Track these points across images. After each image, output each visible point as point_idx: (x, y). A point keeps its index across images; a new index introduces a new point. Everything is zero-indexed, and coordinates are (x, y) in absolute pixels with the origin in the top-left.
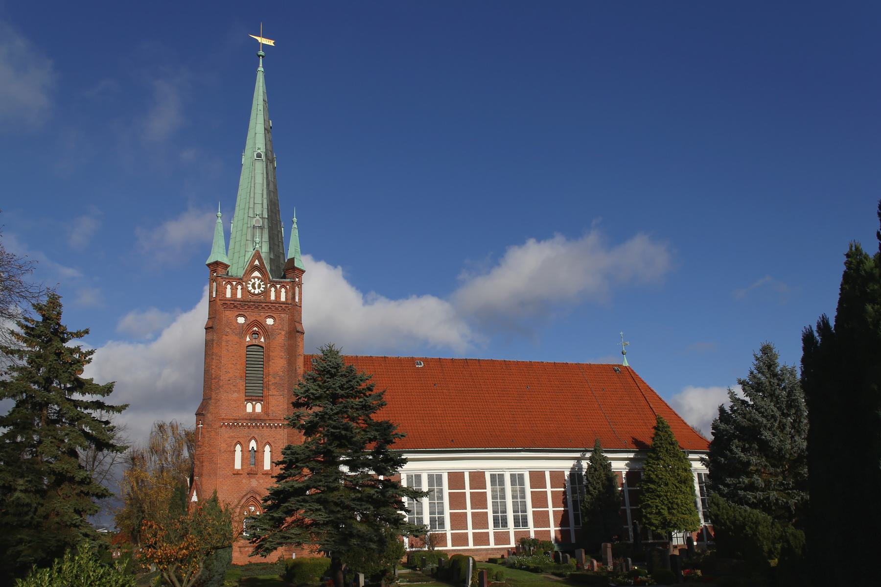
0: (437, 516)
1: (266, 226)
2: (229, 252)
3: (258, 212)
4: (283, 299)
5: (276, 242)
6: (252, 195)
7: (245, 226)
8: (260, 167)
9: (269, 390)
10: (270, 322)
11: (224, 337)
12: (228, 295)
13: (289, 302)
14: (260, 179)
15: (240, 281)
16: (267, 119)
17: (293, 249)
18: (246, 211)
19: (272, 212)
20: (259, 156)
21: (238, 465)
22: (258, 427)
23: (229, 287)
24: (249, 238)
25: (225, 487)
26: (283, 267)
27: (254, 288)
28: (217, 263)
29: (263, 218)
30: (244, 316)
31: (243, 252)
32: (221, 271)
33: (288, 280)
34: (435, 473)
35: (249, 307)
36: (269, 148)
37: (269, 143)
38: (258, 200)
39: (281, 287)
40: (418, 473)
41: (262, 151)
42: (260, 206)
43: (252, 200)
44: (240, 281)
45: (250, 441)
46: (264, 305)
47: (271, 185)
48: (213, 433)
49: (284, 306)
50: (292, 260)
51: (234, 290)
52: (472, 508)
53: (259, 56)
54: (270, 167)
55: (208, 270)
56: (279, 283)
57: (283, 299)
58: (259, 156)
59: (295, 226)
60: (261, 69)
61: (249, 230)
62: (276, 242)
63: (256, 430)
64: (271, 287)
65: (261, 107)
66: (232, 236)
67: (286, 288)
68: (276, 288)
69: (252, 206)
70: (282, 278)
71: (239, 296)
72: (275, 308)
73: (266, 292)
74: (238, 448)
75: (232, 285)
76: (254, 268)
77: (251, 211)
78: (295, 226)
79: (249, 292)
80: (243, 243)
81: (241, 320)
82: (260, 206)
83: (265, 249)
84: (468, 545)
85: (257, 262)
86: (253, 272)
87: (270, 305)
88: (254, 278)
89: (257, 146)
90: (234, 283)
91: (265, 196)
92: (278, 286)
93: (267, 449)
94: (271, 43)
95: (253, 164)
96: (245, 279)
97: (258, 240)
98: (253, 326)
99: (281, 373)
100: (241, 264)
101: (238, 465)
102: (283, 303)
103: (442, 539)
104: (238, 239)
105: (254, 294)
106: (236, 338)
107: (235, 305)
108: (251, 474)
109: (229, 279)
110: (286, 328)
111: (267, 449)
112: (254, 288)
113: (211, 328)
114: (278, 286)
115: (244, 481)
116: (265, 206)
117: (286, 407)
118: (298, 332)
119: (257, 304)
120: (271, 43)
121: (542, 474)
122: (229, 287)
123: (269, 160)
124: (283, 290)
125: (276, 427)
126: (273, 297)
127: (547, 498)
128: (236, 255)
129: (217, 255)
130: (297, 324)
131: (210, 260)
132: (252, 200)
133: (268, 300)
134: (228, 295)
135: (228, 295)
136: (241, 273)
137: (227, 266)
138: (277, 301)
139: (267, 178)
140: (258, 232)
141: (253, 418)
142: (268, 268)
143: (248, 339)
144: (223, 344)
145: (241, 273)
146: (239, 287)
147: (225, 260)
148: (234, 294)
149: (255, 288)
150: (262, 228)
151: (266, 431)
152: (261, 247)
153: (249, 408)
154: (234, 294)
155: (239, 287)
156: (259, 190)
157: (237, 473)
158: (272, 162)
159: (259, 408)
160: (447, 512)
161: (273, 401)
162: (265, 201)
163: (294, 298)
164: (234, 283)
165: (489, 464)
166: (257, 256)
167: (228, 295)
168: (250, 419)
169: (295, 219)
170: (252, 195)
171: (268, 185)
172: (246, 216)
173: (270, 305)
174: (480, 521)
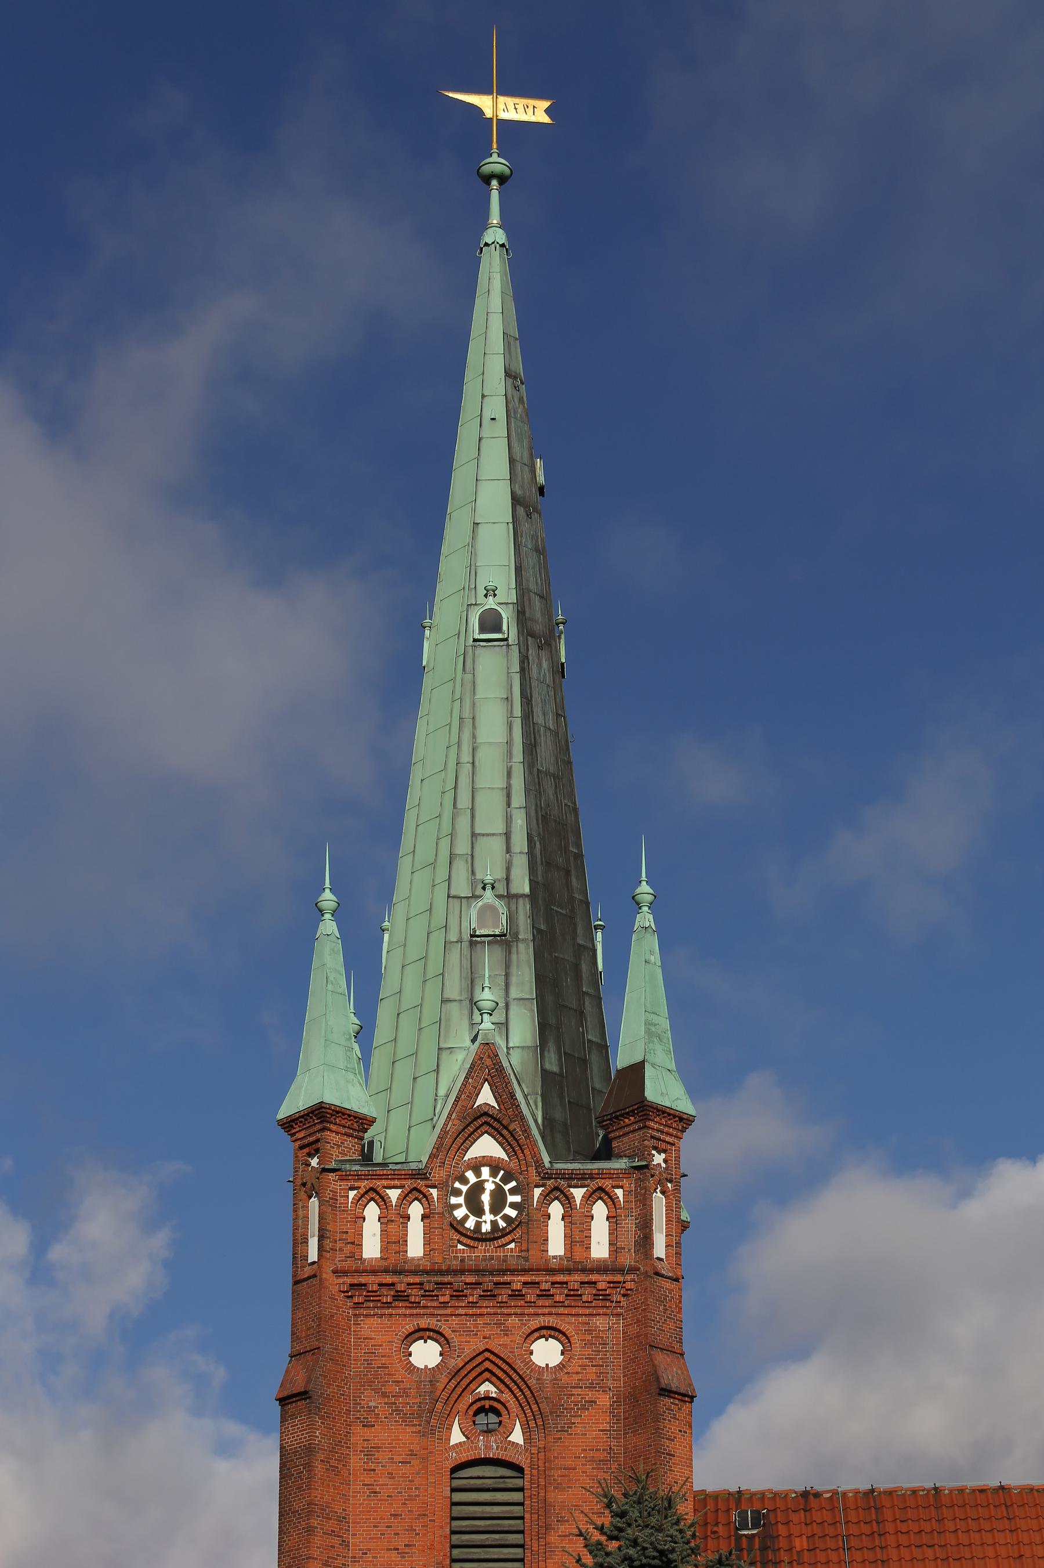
4: (600, 1249)
10: (546, 1353)
11: (359, 1434)
35: (458, 1295)
44: (416, 1182)
46: (517, 1282)
49: (603, 1281)
51: (394, 1223)
56: (580, 1178)
58: (491, 622)
69: (463, 847)
73: (528, 1225)
79: (457, 1226)
81: (426, 1354)
85: (486, 1097)
86: (471, 1138)
91: (518, 798)
106: (407, 1436)
109: (372, 1174)
110: (616, 1377)
114: (578, 1193)
116: (520, 842)
119: (488, 1281)
122: (372, 1211)
126: (556, 1247)
133: (534, 1260)
143: (457, 1436)
144: (356, 1461)
149: (476, 1209)
156: (491, 777)
162: (520, 822)
164: (394, 1194)
170: (464, 802)
171: (531, 747)
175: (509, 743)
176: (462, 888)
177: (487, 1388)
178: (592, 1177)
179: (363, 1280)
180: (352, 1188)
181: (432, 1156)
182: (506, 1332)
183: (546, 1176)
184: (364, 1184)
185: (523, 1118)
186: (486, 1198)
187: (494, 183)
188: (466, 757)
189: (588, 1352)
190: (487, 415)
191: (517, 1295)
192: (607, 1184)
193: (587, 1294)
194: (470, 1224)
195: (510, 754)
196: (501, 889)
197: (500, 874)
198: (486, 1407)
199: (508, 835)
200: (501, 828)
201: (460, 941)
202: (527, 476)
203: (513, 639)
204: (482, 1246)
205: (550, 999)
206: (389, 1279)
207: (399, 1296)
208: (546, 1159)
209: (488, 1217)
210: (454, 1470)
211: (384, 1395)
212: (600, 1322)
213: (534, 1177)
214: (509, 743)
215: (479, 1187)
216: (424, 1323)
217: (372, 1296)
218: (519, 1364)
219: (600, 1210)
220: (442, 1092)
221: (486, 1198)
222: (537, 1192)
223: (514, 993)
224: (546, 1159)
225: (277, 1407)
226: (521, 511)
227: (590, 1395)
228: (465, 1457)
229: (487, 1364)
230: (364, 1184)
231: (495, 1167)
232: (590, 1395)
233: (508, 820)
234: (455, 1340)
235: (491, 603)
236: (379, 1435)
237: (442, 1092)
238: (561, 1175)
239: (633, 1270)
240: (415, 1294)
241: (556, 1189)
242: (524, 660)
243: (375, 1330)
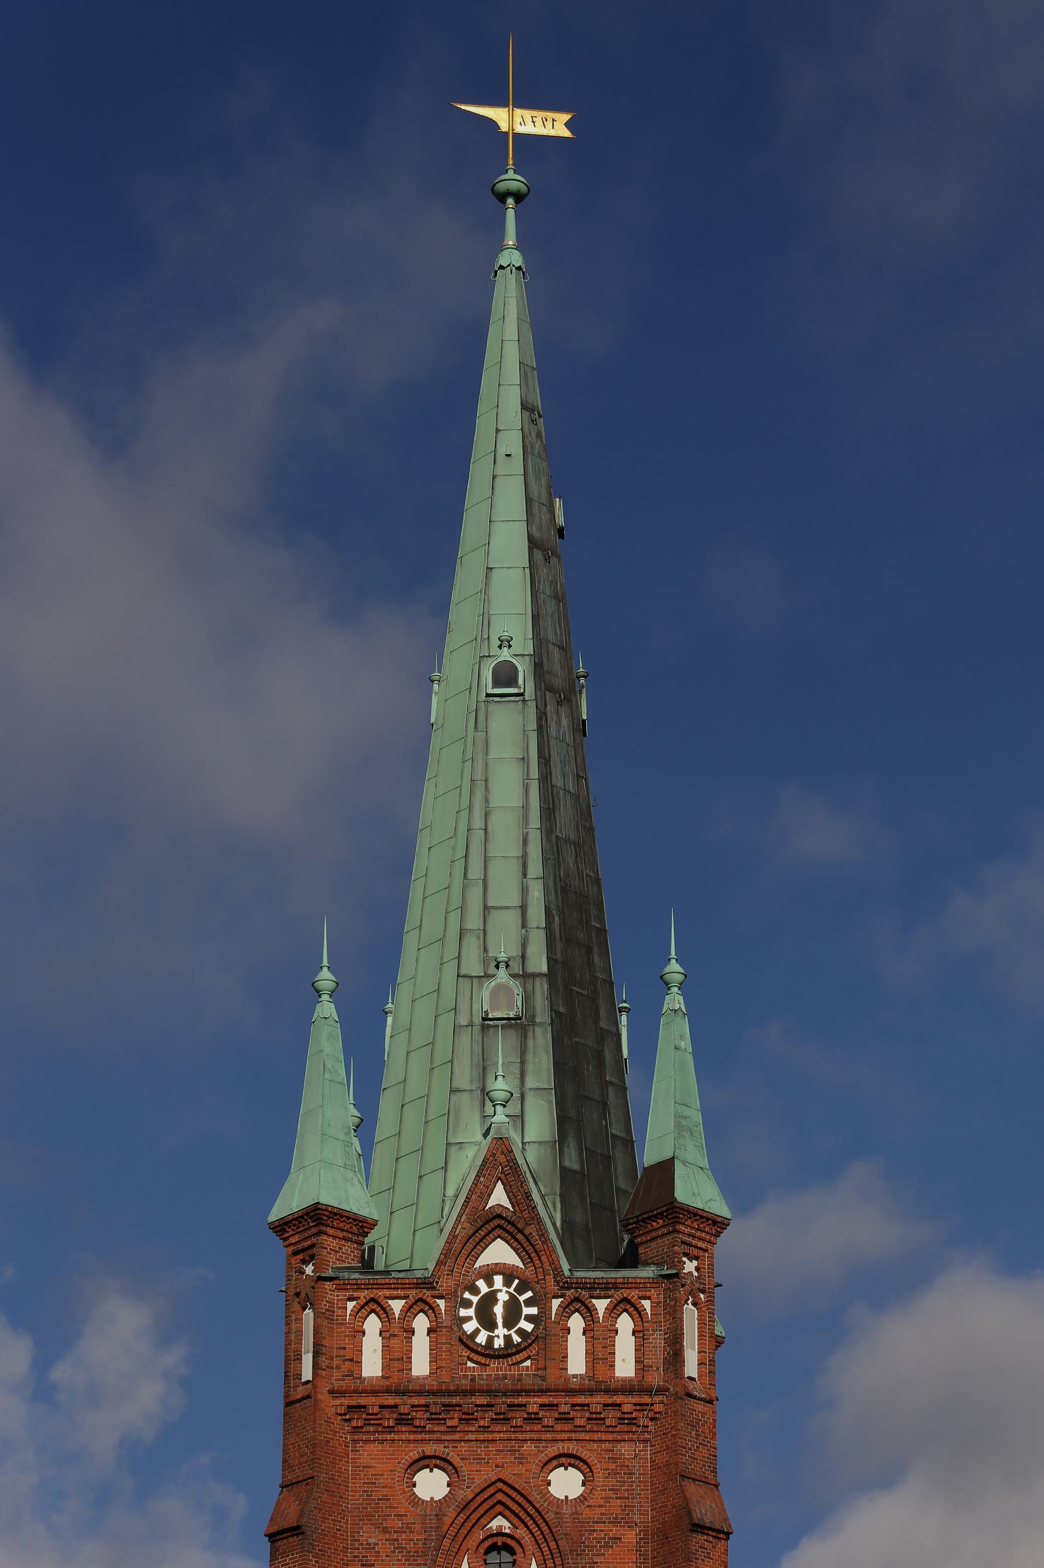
1: (542, 1016)
2: (381, 1155)
3: (504, 948)
4: (625, 1367)
5: (591, 1086)
6: (475, 872)
7: (446, 1022)
8: (511, 730)
10: (566, 1484)
12: (372, 1366)
13: (656, 1379)
14: (511, 788)
15: (422, 1292)
16: (539, 491)
17: (670, 1121)
18: (451, 951)
19: (569, 940)
20: (505, 675)
23: (373, 1324)
24: (464, 1079)
26: (623, 1207)
27: (487, 1321)
28: (317, 1217)
29: (525, 977)
30: (442, 1463)
31: (434, 1156)
32: (336, 1253)
33: (647, 1272)
35: (468, 1418)
36: (551, 632)
37: (549, 608)
38: (505, 890)
39: (613, 1312)
41: (519, 651)
42: (516, 926)
44: (422, 1292)
46: (533, 1403)
47: (565, 813)
49: (628, 1403)
50: (665, 1169)
51: (396, 1336)
53: (502, 197)
54: (560, 725)
55: (277, 1250)
56: (603, 1289)
57: (625, 1367)
58: (505, 675)
59: (675, 1000)
60: (463, 107)
61: (465, 1041)
62: (591, 1086)
64: (567, 1311)
65: (512, 443)
66: (392, 1075)
67: (637, 1313)
68: (589, 1313)
69: (474, 922)
70: (620, 1265)
71: (421, 1365)
72: (593, 1412)
73: (546, 1340)
75: (385, 1313)
76: (487, 1226)
77: (472, 945)
78: (675, 1000)
79: (467, 1341)
80: (438, 1104)
81: (431, 1485)
82: (512, 918)
83: (539, 1123)
85: (499, 1197)
86: (482, 1244)
87: (564, 1404)
88: (488, 1275)
89: (498, 631)
90: (397, 1306)
91: (535, 868)
92: (601, 1305)
94: (555, 125)
95: (479, 721)
96: (445, 1284)
97: (500, 1086)
98: (490, 1513)
100: (429, 1211)
102: (627, 1388)
104: (416, 1085)
105: (488, 1352)
107: (404, 1412)
109: (373, 1284)
110: (643, 1512)
112: (487, 1321)
113: (296, 1530)
114: (601, 1305)
116: (537, 915)
118: (699, 1528)
119: (501, 1403)
120: (555, 125)
122: (373, 1324)
123: (554, 689)
124: (625, 1323)
126: (577, 1364)
128: (408, 1168)
129: (322, 1175)
130: (693, 1490)
131: (289, 1202)
132: (475, 896)
133: (553, 1379)
136: (426, 1256)
137: (362, 1226)
138: (599, 1381)
139: (545, 778)
140: (502, 1047)
142: (550, 1214)
145: (426, 1256)
146: (421, 1323)
147: (353, 1197)
148: (397, 1356)
150: (520, 1025)
152: (519, 1119)
154: (397, 1356)
155: (421, 1323)
156: (505, 844)
158: (567, 698)
162: (537, 894)
163: (675, 1358)
164: (397, 1306)
166: (501, 1165)
167: (372, 1366)
169: (674, 969)
170: (475, 872)
171: (549, 812)
172: (450, 971)
173: (564, 1404)
175: (526, 807)
177: (500, 1523)
178: (615, 1286)
179: (362, 1401)
180: (351, 1299)
181: (440, 1263)
182: (521, 1460)
184: (364, 1295)
185: (539, 1221)
186: (498, 1310)
187: (510, 201)
188: (478, 823)
189: (612, 1482)
190: (502, 451)
191: (533, 1418)
192: (633, 1294)
193: (611, 1417)
197: (515, 951)
199: (523, 908)
200: (515, 901)
201: (471, 1025)
203: (529, 694)
204: (494, 1364)
206: (391, 1400)
207: (403, 1420)
208: (565, 1266)
211: (385, 1530)
212: (625, 1450)
214: (526, 807)
216: (430, 1449)
218: (535, 1496)
219: (625, 1323)
220: (451, 1191)
221: (498, 1310)
222: (556, 1303)
223: (530, 1082)
224: (565, 1266)
226: (538, 555)
227: (614, 1531)
229: (500, 1496)
230: (364, 1295)
232: (614, 1531)
233: (524, 892)
234: (464, 1469)
237: (451, 1191)
239: (662, 1390)
241: (577, 1299)
243: (375, 1457)
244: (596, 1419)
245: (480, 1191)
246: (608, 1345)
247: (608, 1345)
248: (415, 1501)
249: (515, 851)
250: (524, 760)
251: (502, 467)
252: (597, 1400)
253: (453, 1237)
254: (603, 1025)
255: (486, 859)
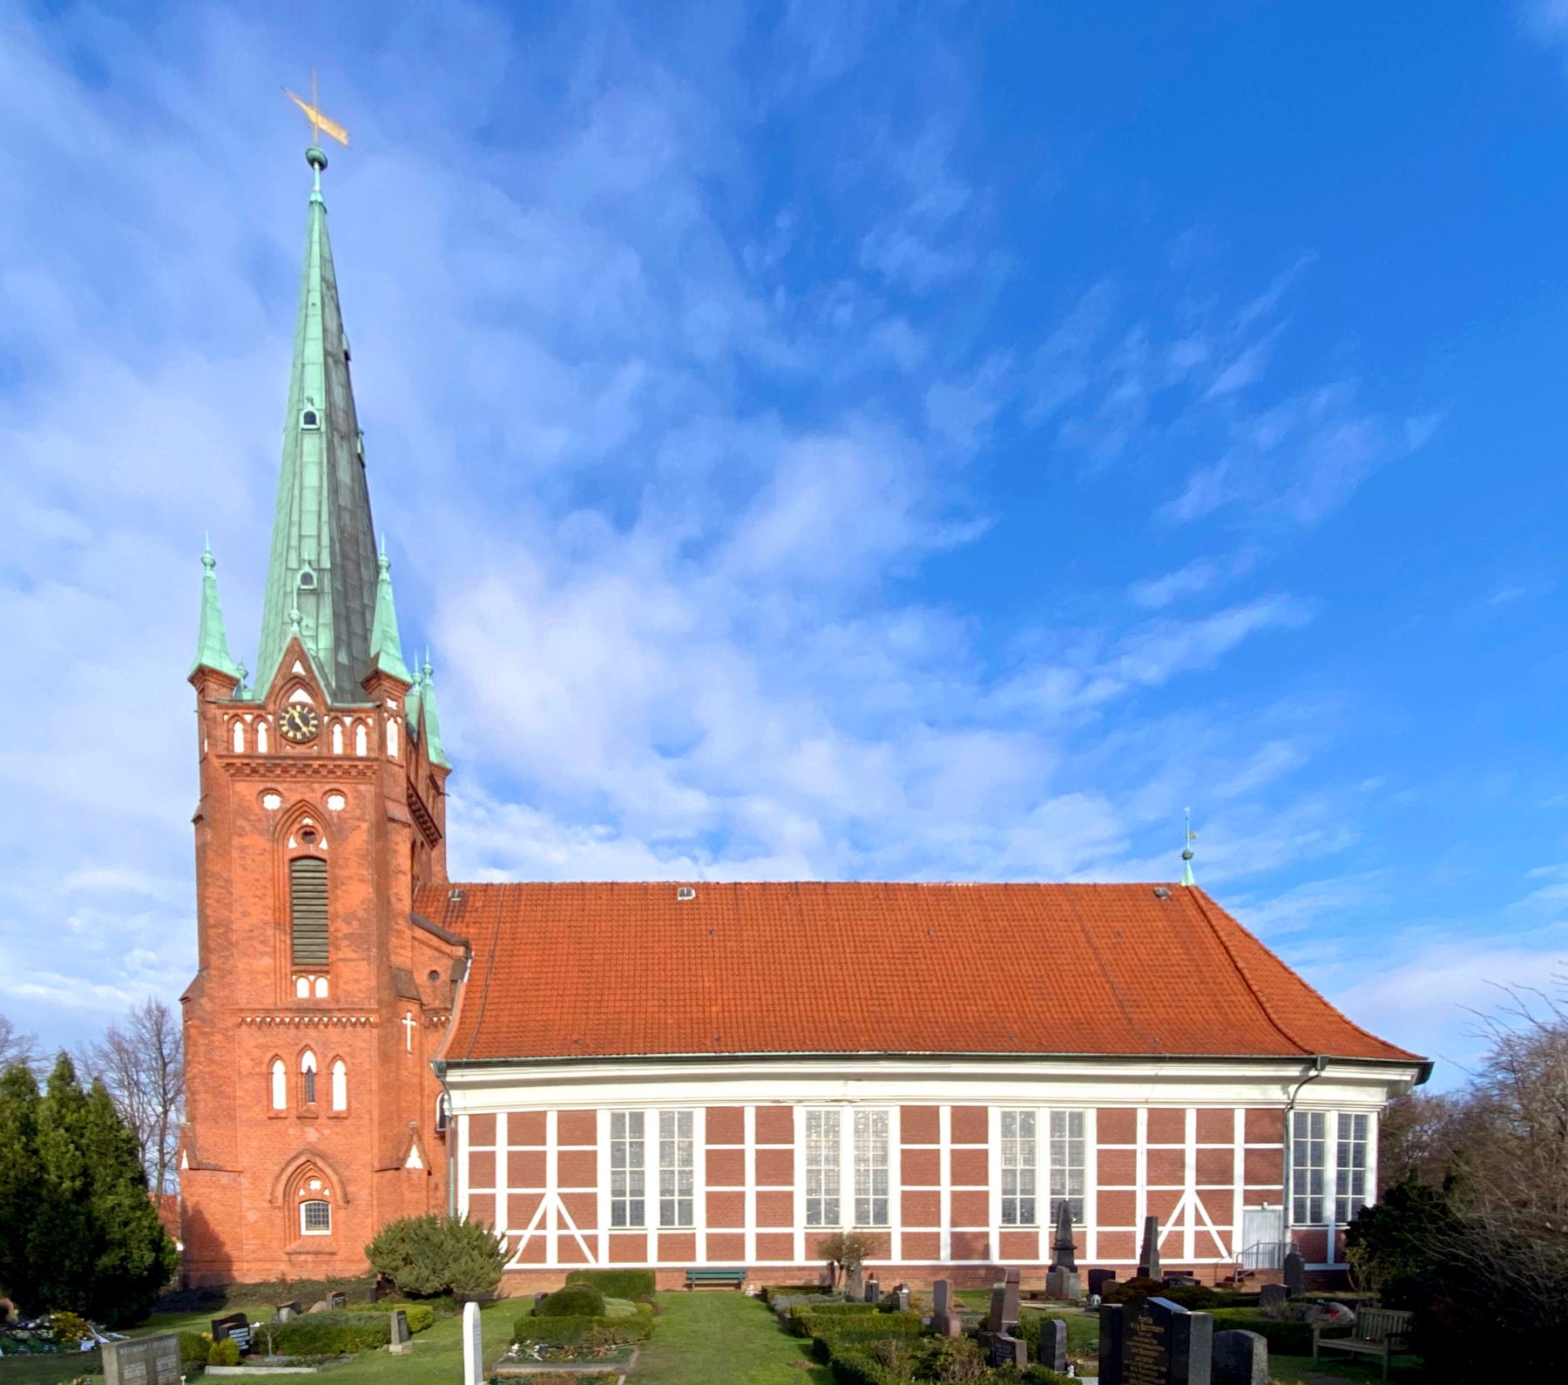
0: (1018, 1196)
4: (361, 751)
9: (338, 948)
10: (336, 803)
11: (236, 841)
21: (280, 1101)
22: (316, 1026)
25: (254, 1144)
27: (297, 728)
30: (339, 792)
34: (1017, 1109)
35: (285, 771)
38: (310, 528)
40: (637, 1109)
41: (318, 407)
43: (295, 530)
44: (259, 710)
45: (301, 1053)
46: (316, 764)
48: (218, 1038)
49: (361, 765)
51: (252, 731)
52: (759, 1183)
56: (348, 712)
58: (310, 418)
63: (311, 1032)
69: (294, 542)
73: (320, 736)
74: (279, 1068)
76: (297, 682)
79: (284, 736)
81: (272, 802)
84: (693, 1258)
86: (291, 690)
87: (238, 762)
88: (294, 706)
91: (325, 517)
93: (339, 1069)
95: (298, 442)
99: (361, 914)
101: (280, 1101)
102: (239, 756)
103: (879, 1245)
105: (295, 742)
106: (262, 842)
107: (251, 767)
108: (304, 1118)
109: (237, 708)
110: (371, 814)
111: (339, 1069)
114: (348, 720)
115: (291, 1131)
116: (325, 541)
117: (374, 983)
119: (300, 763)
121: (491, 1118)
122: (239, 727)
125: (354, 1025)
126: (338, 749)
127: (938, 1164)
132: (295, 530)
133: (325, 752)
134: (239, 747)
135: (239, 747)
138: (251, 754)
141: (312, 1008)
143: (292, 844)
144: (235, 854)
148: (252, 742)
149: (298, 728)
151: (333, 1034)
153: (302, 988)
154: (252, 742)
155: (262, 727)
156: (310, 504)
157: (277, 1117)
159: (322, 988)
160: (700, 1190)
161: (346, 971)
162: (325, 530)
164: (248, 718)
165: (604, 1094)
168: (289, 1010)
170: (295, 518)
171: (334, 490)
173: (330, 765)
174: (583, 1210)
175: (321, 487)
176: (294, 564)
177: (308, 821)
178: (354, 711)
181: (268, 697)
182: (313, 791)
183: (330, 710)
184: (232, 712)
186: (298, 721)
188: (297, 493)
191: (316, 772)
192: (363, 715)
193: (354, 772)
194: (291, 734)
195: (320, 493)
196: (315, 565)
197: (314, 557)
198: (308, 834)
199: (319, 537)
200: (315, 533)
202: (335, 341)
203: (323, 429)
205: (343, 627)
207: (254, 771)
208: (329, 701)
209: (304, 729)
210: (294, 860)
212: (362, 788)
213: (323, 710)
214: (321, 487)
215: (292, 718)
216: (269, 785)
217: (239, 771)
219: (361, 730)
221: (298, 721)
222: (326, 719)
223: (321, 621)
224: (329, 701)
225: (193, 826)
226: (330, 360)
228: (296, 854)
230: (232, 712)
231: (303, 705)
234: (286, 794)
235: (309, 408)
236: (246, 841)
238: (337, 710)
239: (376, 759)
240: (262, 770)
242: (330, 443)
243: (245, 789)
244: (347, 772)
245: (286, 665)
246: (350, 739)
247: (350, 739)
248: (264, 809)
249: (315, 508)
250: (320, 463)
251: (311, 311)
252: (346, 764)
253: (273, 686)
254: (366, 601)
255: (301, 512)
